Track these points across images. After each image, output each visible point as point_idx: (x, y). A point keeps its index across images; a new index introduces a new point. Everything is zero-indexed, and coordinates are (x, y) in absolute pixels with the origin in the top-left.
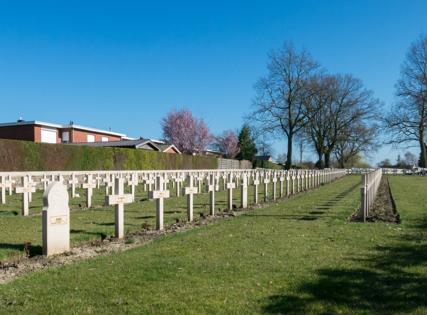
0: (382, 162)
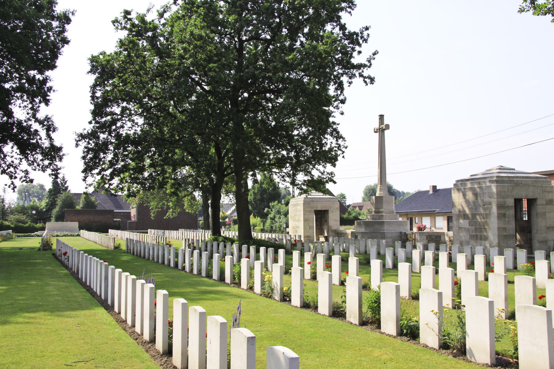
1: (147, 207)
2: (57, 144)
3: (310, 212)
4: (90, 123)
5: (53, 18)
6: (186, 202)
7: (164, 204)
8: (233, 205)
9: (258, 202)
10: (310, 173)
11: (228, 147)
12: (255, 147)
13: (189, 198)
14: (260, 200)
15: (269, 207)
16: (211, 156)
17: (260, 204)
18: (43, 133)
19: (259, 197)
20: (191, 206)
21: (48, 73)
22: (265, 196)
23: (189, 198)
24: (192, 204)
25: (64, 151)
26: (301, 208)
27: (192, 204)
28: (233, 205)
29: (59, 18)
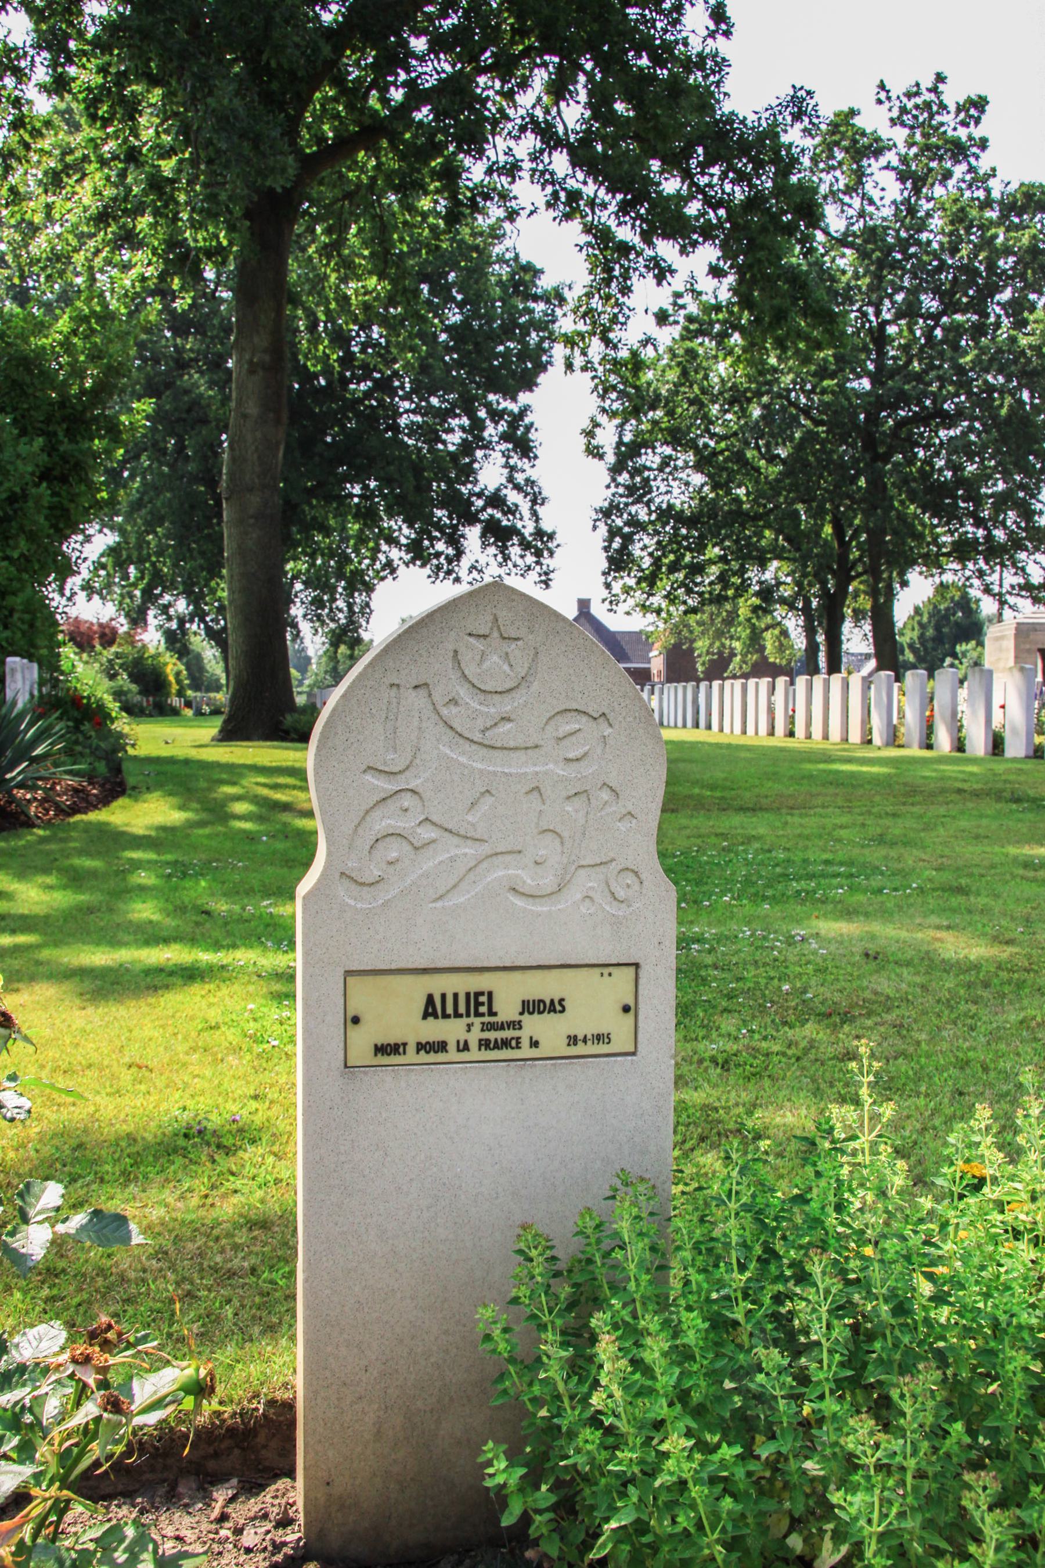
1: (692, 650)
2: (547, 526)
3: (1028, 651)
4: (608, 487)
5: (536, 298)
6: (769, 640)
7: (723, 645)
8: (867, 657)
9: (930, 645)
10: (1023, 569)
11: (857, 522)
13: (777, 632)
15: (954, 655)
17: (934, 649)
18: (525, 506)
19: (930, 632)
20: (781, 648)
21: (524, 398)
22: (946, 630)
23: (777, 632)
24: (781, 645)
25: (559, 539)
26: (1010, 644)
27: (781, 645)
28: (867, 657)
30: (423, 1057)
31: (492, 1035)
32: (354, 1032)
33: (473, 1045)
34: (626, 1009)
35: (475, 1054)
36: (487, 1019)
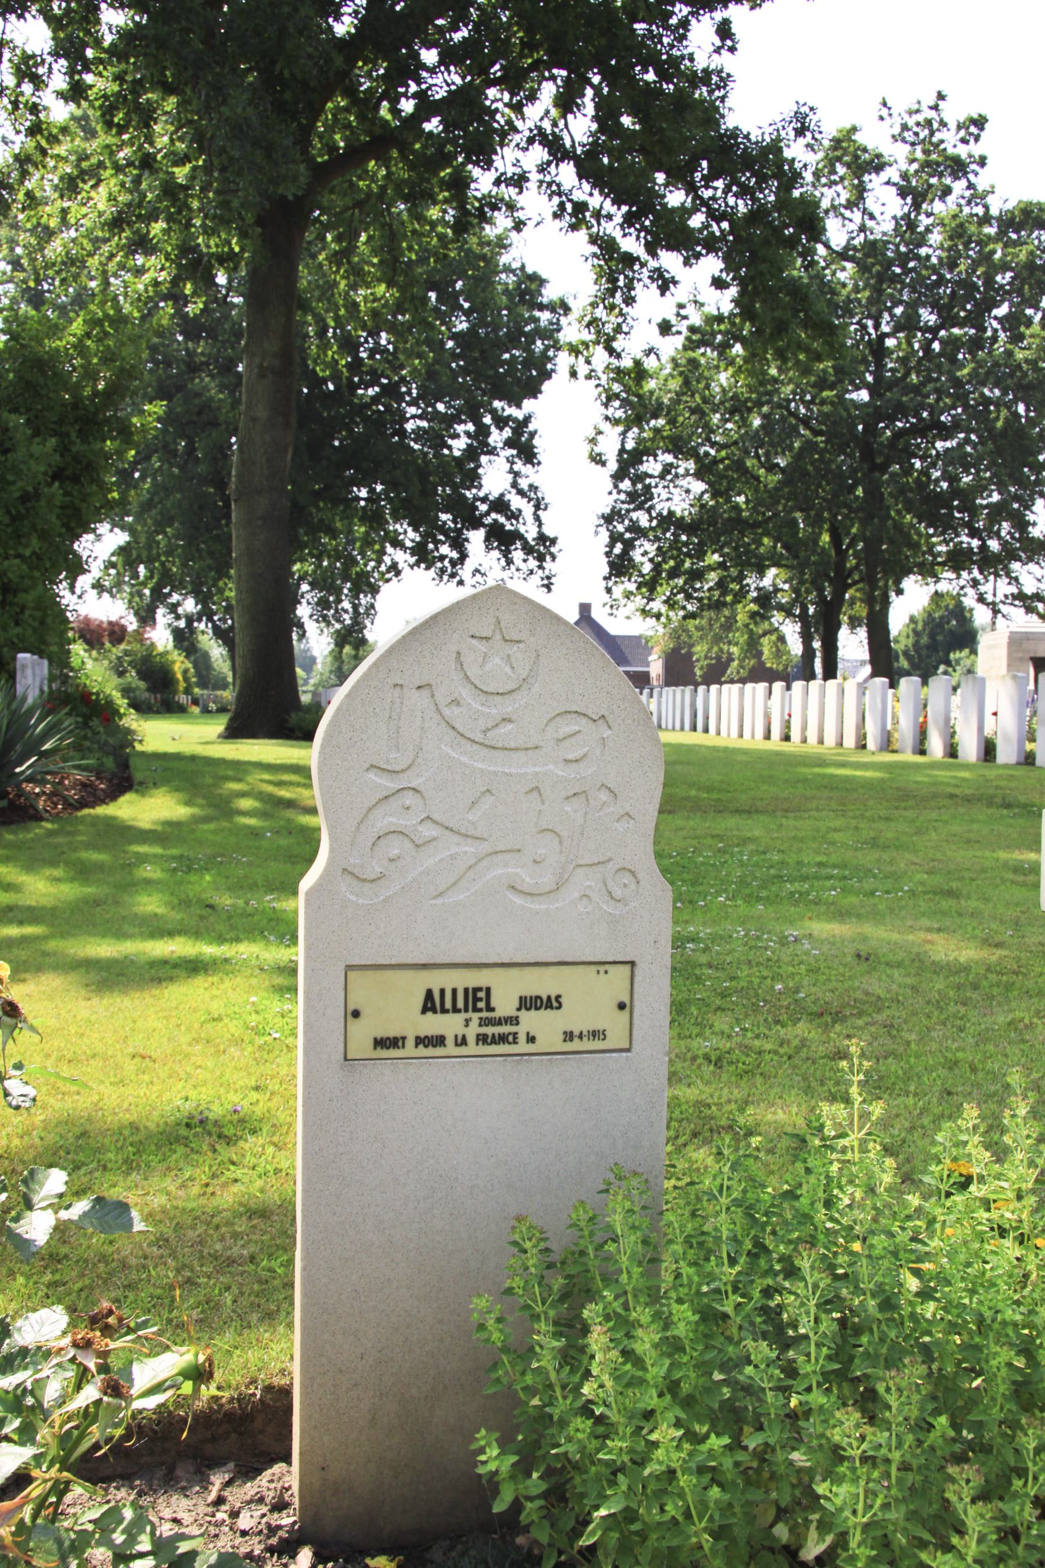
0: (24, 980)
1: (690, 654)
2: (549, 531)
3: (1021, 660)
5: (541, 307)
6: (766, 645)
7: (721, 650)
9: (924, 652)
11: (854, 530)
12: (901, 531)
13: (774, 638)
14: (928, 647)
15: (948, 663)
16: (823, 549)
17: (929, 657)
19: (925, 640)
21: (528, 405)
22: (940, 638)
24: (778, 650)
26: (1003, 652)
27: (778, 650)
28: (863, 663)
29: (551, 307)
30: (422, 1051)
31: (490, 1030)
32: (354, 1025)
33: (471, 1039)
34: (622, 1006)
35: (472, 1048)
36: (484, 1014)
